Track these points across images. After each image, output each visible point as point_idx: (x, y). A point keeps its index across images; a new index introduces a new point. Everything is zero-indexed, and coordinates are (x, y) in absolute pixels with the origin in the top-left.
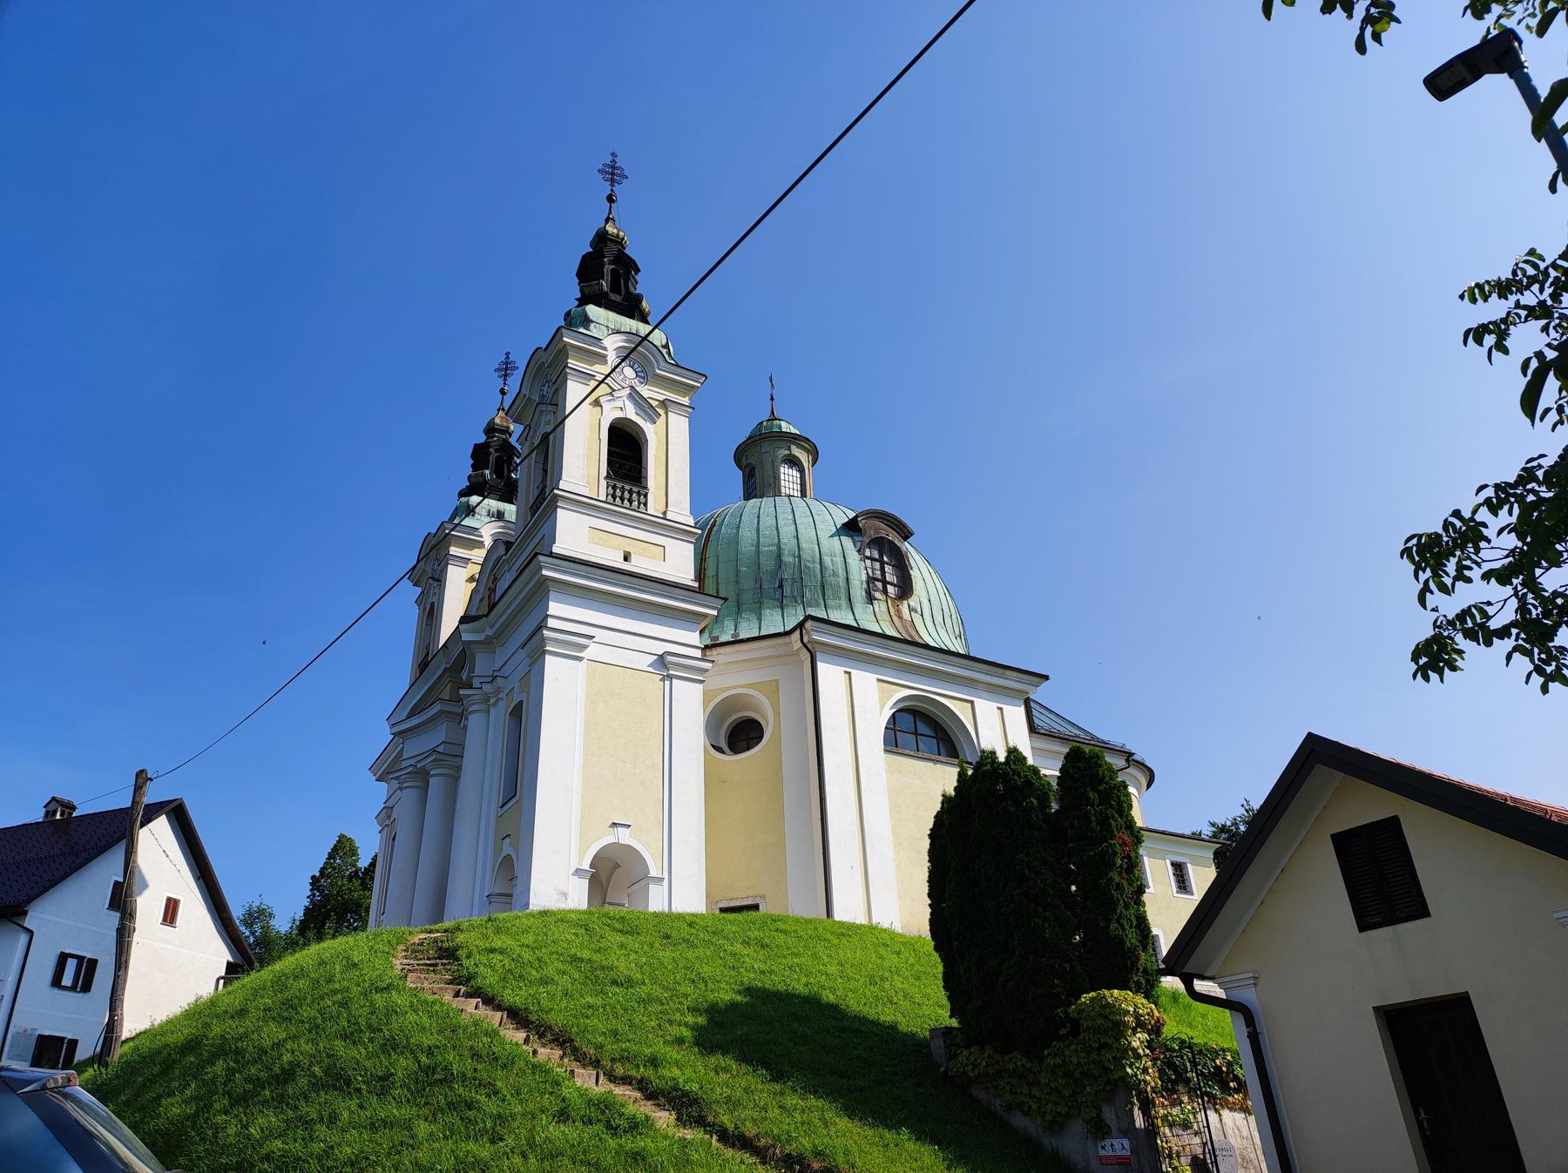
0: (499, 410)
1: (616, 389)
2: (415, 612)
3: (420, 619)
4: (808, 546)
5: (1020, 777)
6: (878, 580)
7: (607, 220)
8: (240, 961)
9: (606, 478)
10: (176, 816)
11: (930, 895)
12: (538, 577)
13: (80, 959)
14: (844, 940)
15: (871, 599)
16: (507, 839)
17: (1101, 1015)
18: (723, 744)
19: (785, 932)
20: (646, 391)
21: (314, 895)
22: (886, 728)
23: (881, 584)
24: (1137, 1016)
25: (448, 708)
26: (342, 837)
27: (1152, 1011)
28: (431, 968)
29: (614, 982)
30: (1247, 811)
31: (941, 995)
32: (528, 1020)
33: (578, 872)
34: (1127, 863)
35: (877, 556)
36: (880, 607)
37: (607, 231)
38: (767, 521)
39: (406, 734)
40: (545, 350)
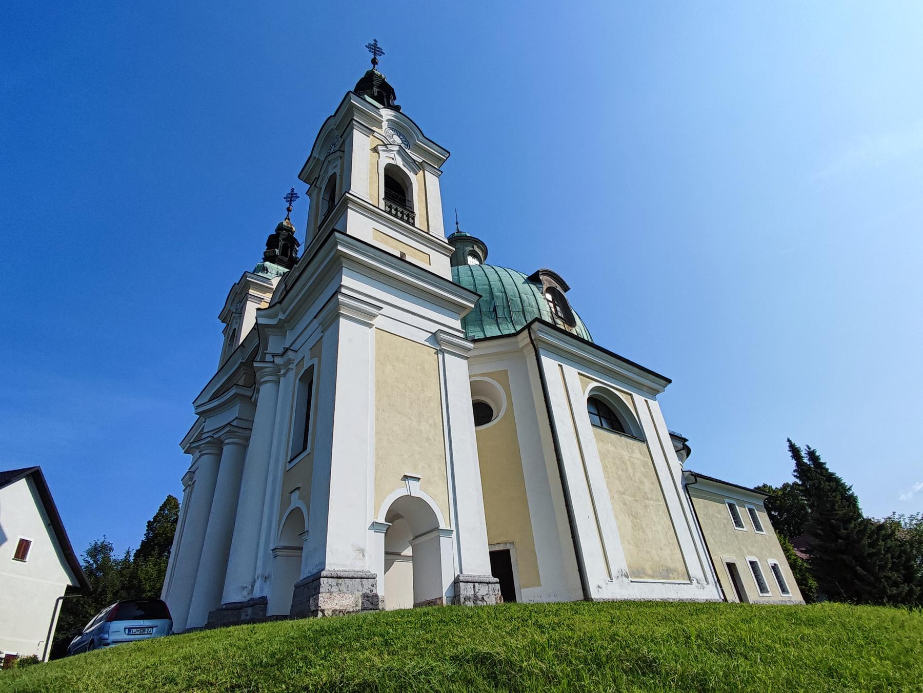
8: (78, 586)
10: (33, 478)
12: (335, 250)
16: (297, 493)
21: (149, 533)
25: (242, 391)
26: (170, 496)
33: (375, 526)
39: (208, 413)
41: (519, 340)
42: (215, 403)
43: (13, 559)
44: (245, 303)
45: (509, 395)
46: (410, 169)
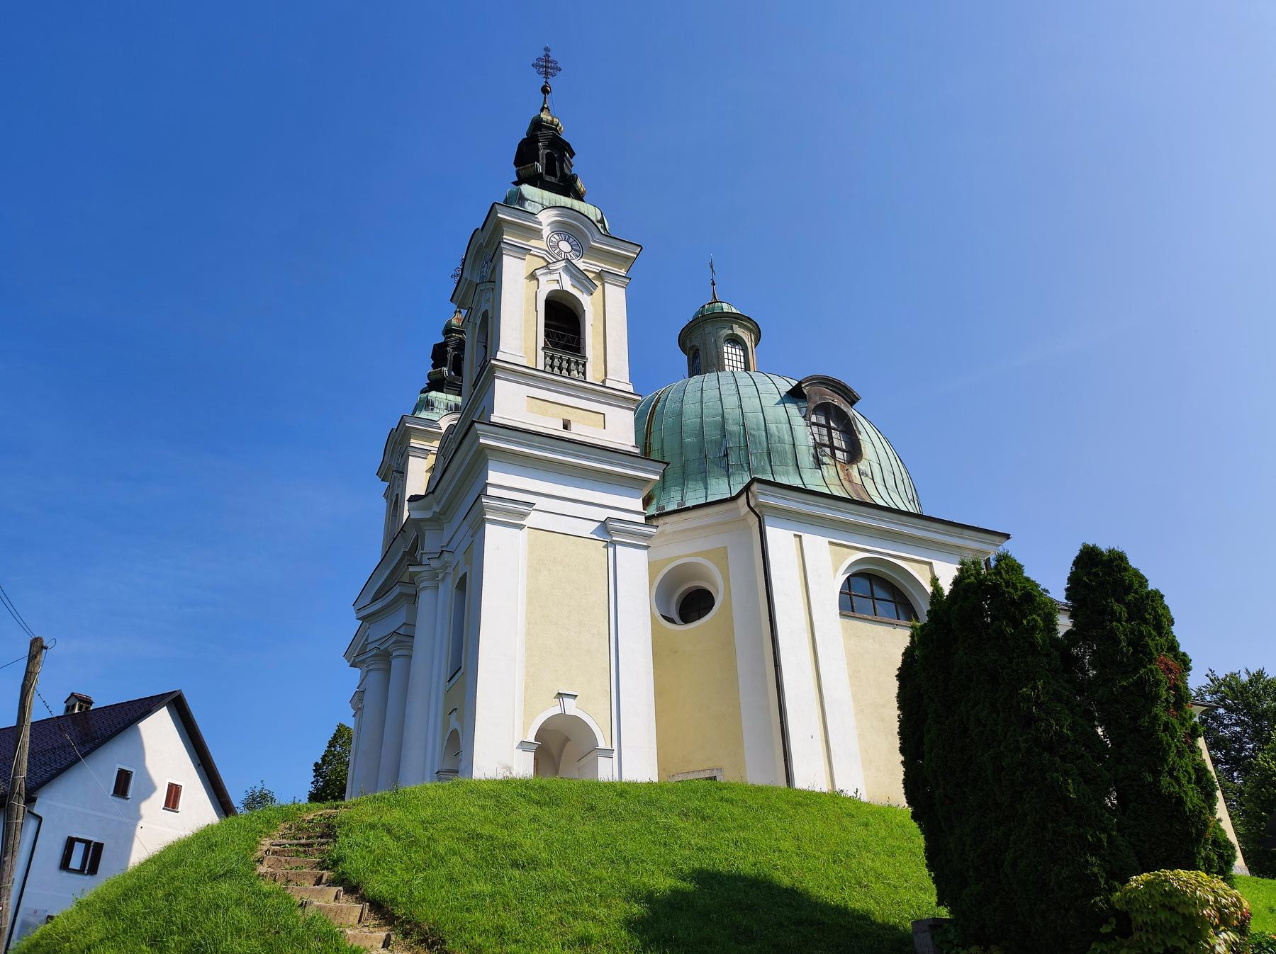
0: (455, 313)
1: (551, 262)
2: (383, 504)
3: (388, 513)
4: (754, 418)
5: (1016, 589)
6: (825, 445)
7: (542, 110)
9: (543, 348)
11: (902, 750)
12: (477, 444)
13: (88, 843)
14: (801, 811)
15: (819, 464)
17: (1163, 906)
18: (674, 614)
19: (731, 801)
20: (580, 264)
22: (841, 593)
23: (829, 449)
24: (1220, 909)
27: (1238, 899)
28: (301, 849)
29: (515, 864)
30: (1212, 681)
31: (922, 874)
32: (393, 915)
33: (523, 745)
34: (1174, 696)
35: (823, 422)
36: (829, 471)
37: (542, 118)
38: (710, 394)
40: (482, 229)
41: (740, 506)
42: (378, 605)
43: (163, 809)
44: (407, 460)
45: (727, 579)
46: (583, 290)
